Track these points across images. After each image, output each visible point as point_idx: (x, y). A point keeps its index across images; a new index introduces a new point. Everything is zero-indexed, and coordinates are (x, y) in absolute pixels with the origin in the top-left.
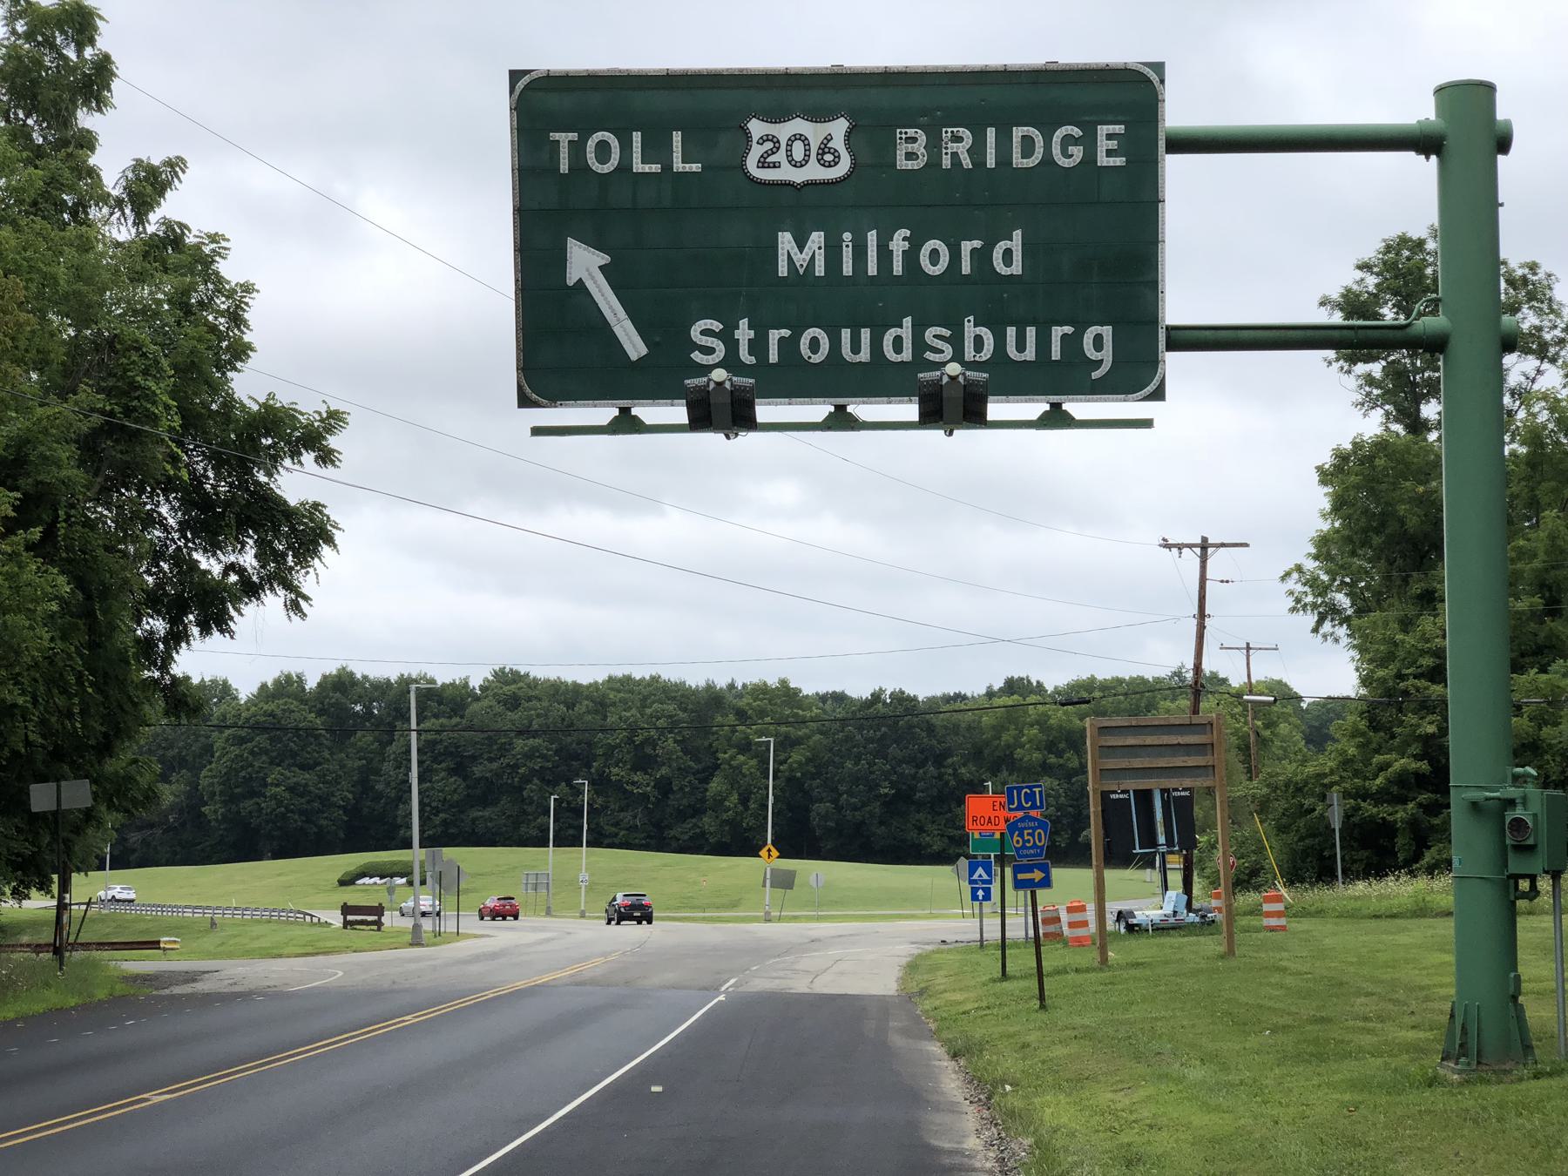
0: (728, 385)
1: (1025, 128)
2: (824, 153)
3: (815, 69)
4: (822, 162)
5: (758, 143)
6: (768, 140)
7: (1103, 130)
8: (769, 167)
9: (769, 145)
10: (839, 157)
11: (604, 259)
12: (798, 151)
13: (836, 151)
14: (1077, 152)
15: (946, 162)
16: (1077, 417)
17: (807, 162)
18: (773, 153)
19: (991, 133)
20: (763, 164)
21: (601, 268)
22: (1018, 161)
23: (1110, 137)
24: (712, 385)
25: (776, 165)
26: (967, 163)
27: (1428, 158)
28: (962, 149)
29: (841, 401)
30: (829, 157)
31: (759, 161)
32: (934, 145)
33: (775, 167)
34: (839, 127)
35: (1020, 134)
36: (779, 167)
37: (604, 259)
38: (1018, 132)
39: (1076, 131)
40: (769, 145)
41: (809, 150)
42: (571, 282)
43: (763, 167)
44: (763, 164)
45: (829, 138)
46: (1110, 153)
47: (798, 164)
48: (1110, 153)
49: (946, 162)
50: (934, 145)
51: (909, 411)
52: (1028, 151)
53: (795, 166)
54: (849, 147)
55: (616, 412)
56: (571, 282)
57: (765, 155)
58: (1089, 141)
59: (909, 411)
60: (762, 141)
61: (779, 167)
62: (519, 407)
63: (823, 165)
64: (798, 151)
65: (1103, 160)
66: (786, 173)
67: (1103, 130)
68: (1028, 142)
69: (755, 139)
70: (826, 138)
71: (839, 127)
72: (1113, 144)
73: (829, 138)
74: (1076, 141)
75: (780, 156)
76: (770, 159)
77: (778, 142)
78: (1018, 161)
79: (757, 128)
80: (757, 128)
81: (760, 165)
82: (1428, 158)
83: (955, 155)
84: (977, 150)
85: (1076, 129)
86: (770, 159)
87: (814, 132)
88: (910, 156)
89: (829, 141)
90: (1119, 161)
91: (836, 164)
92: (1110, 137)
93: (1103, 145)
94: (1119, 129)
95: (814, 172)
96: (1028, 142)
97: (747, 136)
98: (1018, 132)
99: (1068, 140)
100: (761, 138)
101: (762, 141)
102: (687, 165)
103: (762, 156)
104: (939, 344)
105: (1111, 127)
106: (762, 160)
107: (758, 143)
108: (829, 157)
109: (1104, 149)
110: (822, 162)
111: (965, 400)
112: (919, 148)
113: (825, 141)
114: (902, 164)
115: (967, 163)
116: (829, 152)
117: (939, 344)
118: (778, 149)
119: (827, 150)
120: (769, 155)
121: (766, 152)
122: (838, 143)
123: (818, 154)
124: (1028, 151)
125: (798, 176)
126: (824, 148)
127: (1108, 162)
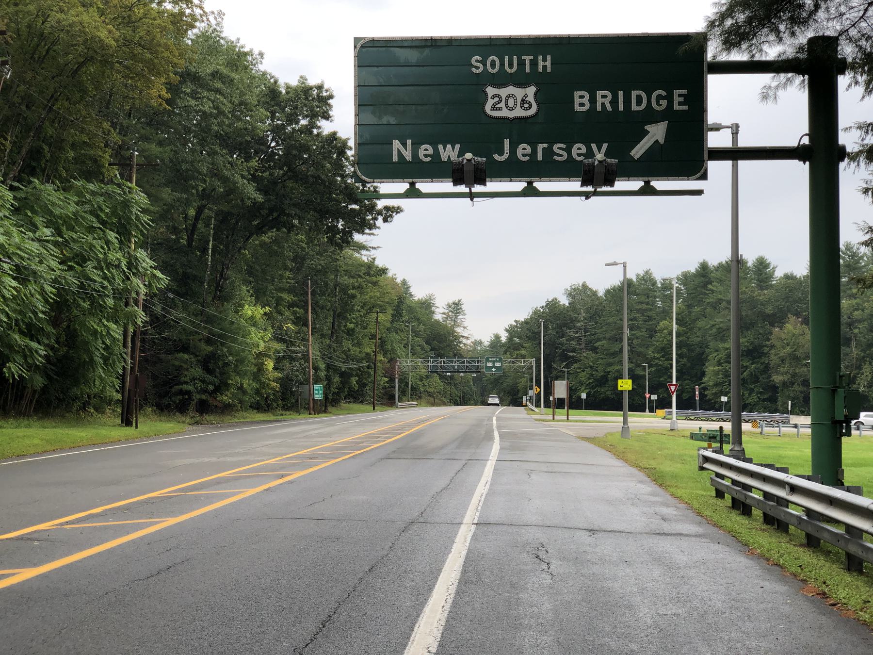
3: (476, 36)
6: (508, 98)
7: (677, 92)
8: (496, 110)
9: (497, 99)
10: (531, 105)
11: (662, 141)
12: (511, 103)
13: (530, 102)
14: (664, 103)
15: (599, 108)
16: (424, 191)
18: (499, 103)
19: (621, 93)
20: (494, 108)
22: (634, 107)
23: (680, 96)
24: (465, 161)
25: (500, 109)
26: (609, 108)
27: (804, 163)
28: (607, 101)
33: (499, 110)
34: (531, 90)
37: (662, 141)
38: (634, 93)
39: (664, 93)
40: (497, 99)
42: (647, 127)
43: (494, 110)
44: (494, 108)
46: (680, 104)
48: (680, 104)
49: (599, 108)
50: (593, 100)
52: (639, 102)
54: (536, 101)
56: (647, 127)
58: (670, 98)
65: (676, 107)
66: (505, 113)
67: (677, 92)
68: (639, 98)
69: (490, 96)
70: (524, 96)
71: (531, 90)
72: (682, 99)
73: (526, 96)
74: (663, 98)
75: (502, 105)
77: (501, 97)
79: (490, 91)
80: (490, 91)
82: (804, 163)
83: (603, 104)
84: (614, 102)
85: (479, 57)
87: (519, 93)
89: (526, 97)
90: (685, 107)
92: (680, 96)
93: (677, 99)
94: (684, 91)
95: (519, 112)
96: (639, 98)
97: (486, 94)
98: (634, 93)
99: (659, 97)
100: (493, 96)
101: (494, 96)
104: (561, 152)
105: (680, 91)
108: (526, 105)
111: (475, 173)
112: (586, 100)
115: (609, 108)
117: (561, 152)
118: (501, 101)
120: (497, 104)
122: (531, 98)
123: (521, 104)
124: (639, 102)
125: (511, 115)
126: (523, 101)
127: (580, 109)
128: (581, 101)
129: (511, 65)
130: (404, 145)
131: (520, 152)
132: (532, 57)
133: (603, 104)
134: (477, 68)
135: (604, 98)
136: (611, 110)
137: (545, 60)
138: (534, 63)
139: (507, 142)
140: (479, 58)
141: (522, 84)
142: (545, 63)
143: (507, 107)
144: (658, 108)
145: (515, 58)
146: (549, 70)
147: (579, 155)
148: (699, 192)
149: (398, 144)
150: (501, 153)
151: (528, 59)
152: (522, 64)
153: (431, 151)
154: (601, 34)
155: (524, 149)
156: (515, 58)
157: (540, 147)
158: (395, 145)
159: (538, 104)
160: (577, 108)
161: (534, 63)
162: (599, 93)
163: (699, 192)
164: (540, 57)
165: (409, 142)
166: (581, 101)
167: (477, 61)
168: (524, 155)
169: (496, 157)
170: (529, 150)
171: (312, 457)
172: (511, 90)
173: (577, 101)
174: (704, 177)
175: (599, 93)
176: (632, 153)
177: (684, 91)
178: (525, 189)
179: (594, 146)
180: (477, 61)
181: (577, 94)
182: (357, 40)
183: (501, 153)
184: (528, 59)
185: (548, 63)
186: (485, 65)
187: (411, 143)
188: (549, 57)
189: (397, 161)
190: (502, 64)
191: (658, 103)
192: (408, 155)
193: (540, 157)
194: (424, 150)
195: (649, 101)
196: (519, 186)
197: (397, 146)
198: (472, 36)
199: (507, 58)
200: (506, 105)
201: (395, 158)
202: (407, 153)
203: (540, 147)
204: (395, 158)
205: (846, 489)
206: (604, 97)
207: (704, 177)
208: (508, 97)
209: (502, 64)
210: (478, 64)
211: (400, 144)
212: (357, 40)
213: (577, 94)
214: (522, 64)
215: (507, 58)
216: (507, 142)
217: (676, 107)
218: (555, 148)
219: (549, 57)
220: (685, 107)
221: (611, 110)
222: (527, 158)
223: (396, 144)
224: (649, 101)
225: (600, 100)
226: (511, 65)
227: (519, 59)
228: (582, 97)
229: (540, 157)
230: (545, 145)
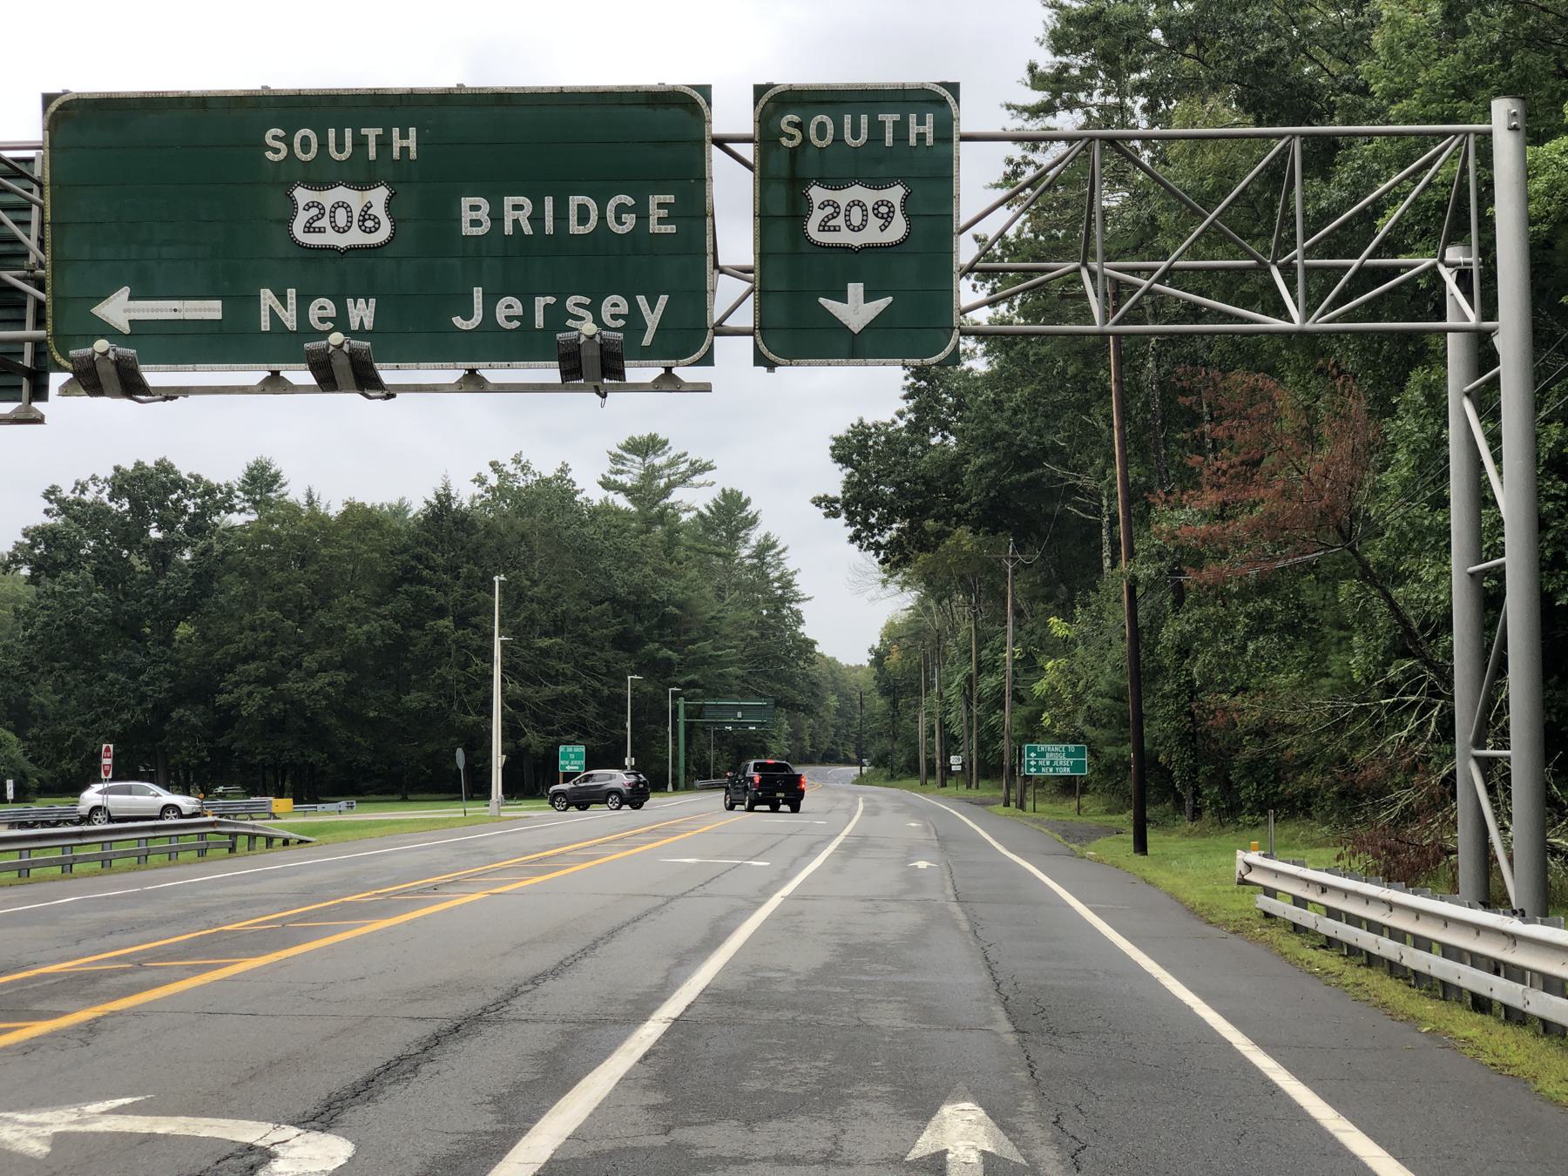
0: (111, 355)
1: (581, 197)
2: (364, 220)
4: (363, 228)
5: (819, 208)
7: (654, 200)
8: (829, 230)
10: (379, 223)
11: (125, 291)
12: (341, 217)
13: (376, 217)
14: (630, 220)
15: (508, 229)
16: (686, 381)
17: (350, 228)
18: (319, 219)
21: (131, 298)
22: (575, 228)
23: (660, 206)
26: (527, 229)
28: (523, 216)
29: (275, 367)
30: (369, 224)
31: (820, 225)
32: (497, 217)
34: (379, 196)
35: (576, 203)
36: (325, 232)
37: (125, 291)
38: (575, 201)
41: (352, 217)
45: (369, 206)
46: (661, 221)
47: (341, 230)
48: (661, 221)
49: (508, 229)
50: (497, 217)
51: (552, 374)
52: (583, 218)
53: (338, 231)
55: (662, 371)
57: (826, 219)
59: (552, 374)
60: (308, 207)
61: (325, 232)
62: (755, 365)
63: (364, 231)
64: (341, 217)
65: (654, 227)
66: (845, 237)
67: (654, 200)
68: (582, 212)
69: (816, 206)
71: (379, 196)
72: (664, 213)
73: (369, 206)
75: (324, 222)
76: (316, 224)
77: (838, 207)
78: (575, 228)
79: (302, 195)
80: (302, 195)
81: (821, 228)
83: (516, 222)
84: (537, 218)
86: (316, 224)
87: (355, 198)
88: (476, 223)
89: (369, 208)
90: (671, 229)
91: (377, 229)
92: (660, 206)
93: (655, 213)
94: (670, 198)
95: (356, 237)
96: (582, 212)
97: (293, 203)
98: (575, 201)
99: (621, 209)
102: (663, 227)
103: (308, 222)
105: (662, 197)
106: (308, 225)
107: (819, 208)
108: (369, 224)
109: (656, 217)
110: (363, 228)
112: (483, 214)
113: (880, 203)
114: (467, 230)
115: (527, 229)
116: (370, 219)
118: (838, 213)
119: (367, 217)
121: (827, 216)
122: (379, 210)
124: (583, 218)
125: (342, 241)
126: (365, 216)
127: (660, 229)
128: (473, 215)
129: (340, 147)
130: (282, 298)
131: (501, 312)
132: (380, 131)
133: (516, 222)
134: (277, 151)
135: (517, 211)
136: (531, 233)
137: (404, 136)
138: (384, 143)
139: (478, 293)
140: (280, 132)
141: (363, 184)
142: (406, 142)
143: (848, 226)
144: (620, 230)
145: (348, 132)
146: (413, 155)
147: (615, 317)
148: (706, 388)
149: (270, 298)
150: (468, 316)
151: (372, 133)
152: (361, 142)
153: (624, 308)
154: (575, 87)
155: (509, 307)
156: (348, 132)
157: (540, 302)
158: (265, 299)
159: (395, 224)
160: (467, 230)
161: (384, 143)
162: (509, 201)
163: (706, 388)
164: (396, 131)
165: (291, 293)
166: (475, 215)
167: (275, 138)
168: (509, 318)
169: (458, 321)
170: (518, 309)
171: (242, 904)
172: (341, 193)
173: (467, 215)
174: (707, 360)
175: (509, 201)
176: (218, 316)
177: (670, 198)
178: (266, 381)
179: (642, 300)
180: (275, 138)
181: (466, 202)
182: (48, 99)
183: (468, 316)
184: (372, 133)
185: (412, 143)
186: (290, 146)
187: (294, 296)
188: (412, 131)
189: (542, 326)
190: (323, 145)
191: (619, 220)
192: (290, 319)
193: (539, 321)
194: (319, 309)
195: (602, 217)
196: (255, 375)
197: (269, 302)
198: (627, 87)
199: (332, 133)
200: (846, 221)
201: (265, 325)
202: (287, 315)
203: (540, 302)
204: (265, 325)
205: (1408, 937)
206: (518, 207)
207: (707, 360)
208: (336, 206)
209: (323, 145)
210: (278, 144)
211: (274, 298)
212: (48, 99)
213: (466, 202)
214: (361, 142)
215: (332, 133)
216: (478, 293)
217: (654, 227)
218: (570, 302)
219: (412, 131)
220: (671, 229)
221: (531, 233)
222: (516, 324)
223: (267, 297)
224: (602, 217)
225: (509, 216)
226: (340, 147)
227: (356, 135)
228: (475, 208)
229: (539, 321)
230: (551, 300)
